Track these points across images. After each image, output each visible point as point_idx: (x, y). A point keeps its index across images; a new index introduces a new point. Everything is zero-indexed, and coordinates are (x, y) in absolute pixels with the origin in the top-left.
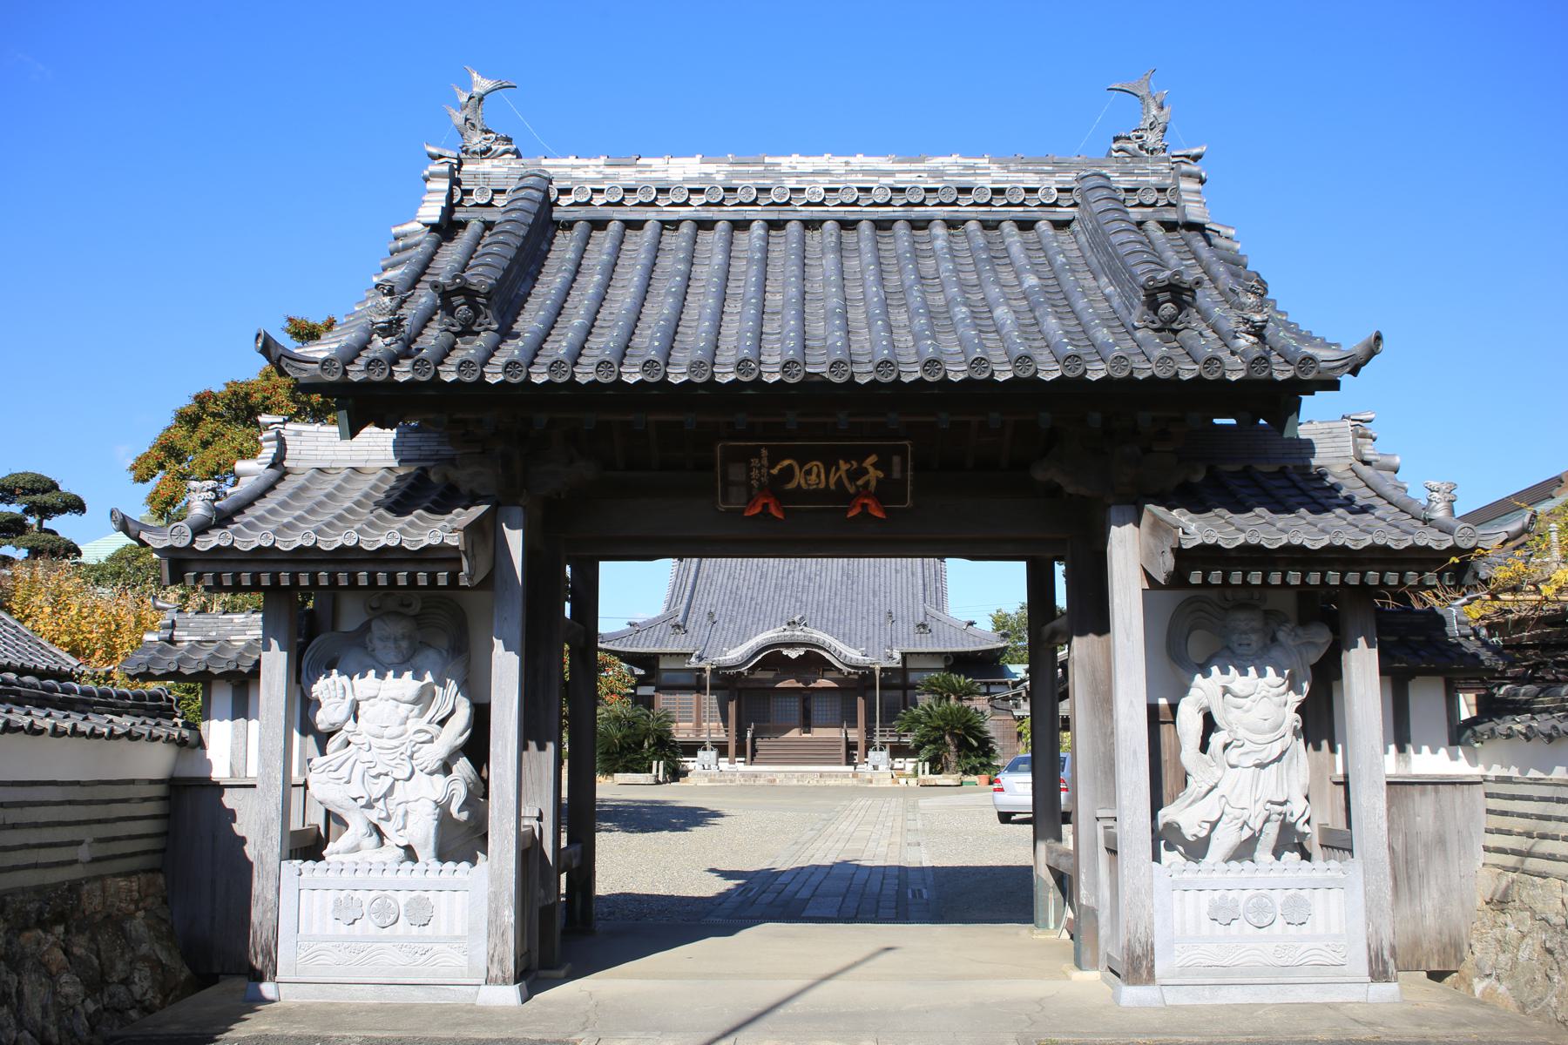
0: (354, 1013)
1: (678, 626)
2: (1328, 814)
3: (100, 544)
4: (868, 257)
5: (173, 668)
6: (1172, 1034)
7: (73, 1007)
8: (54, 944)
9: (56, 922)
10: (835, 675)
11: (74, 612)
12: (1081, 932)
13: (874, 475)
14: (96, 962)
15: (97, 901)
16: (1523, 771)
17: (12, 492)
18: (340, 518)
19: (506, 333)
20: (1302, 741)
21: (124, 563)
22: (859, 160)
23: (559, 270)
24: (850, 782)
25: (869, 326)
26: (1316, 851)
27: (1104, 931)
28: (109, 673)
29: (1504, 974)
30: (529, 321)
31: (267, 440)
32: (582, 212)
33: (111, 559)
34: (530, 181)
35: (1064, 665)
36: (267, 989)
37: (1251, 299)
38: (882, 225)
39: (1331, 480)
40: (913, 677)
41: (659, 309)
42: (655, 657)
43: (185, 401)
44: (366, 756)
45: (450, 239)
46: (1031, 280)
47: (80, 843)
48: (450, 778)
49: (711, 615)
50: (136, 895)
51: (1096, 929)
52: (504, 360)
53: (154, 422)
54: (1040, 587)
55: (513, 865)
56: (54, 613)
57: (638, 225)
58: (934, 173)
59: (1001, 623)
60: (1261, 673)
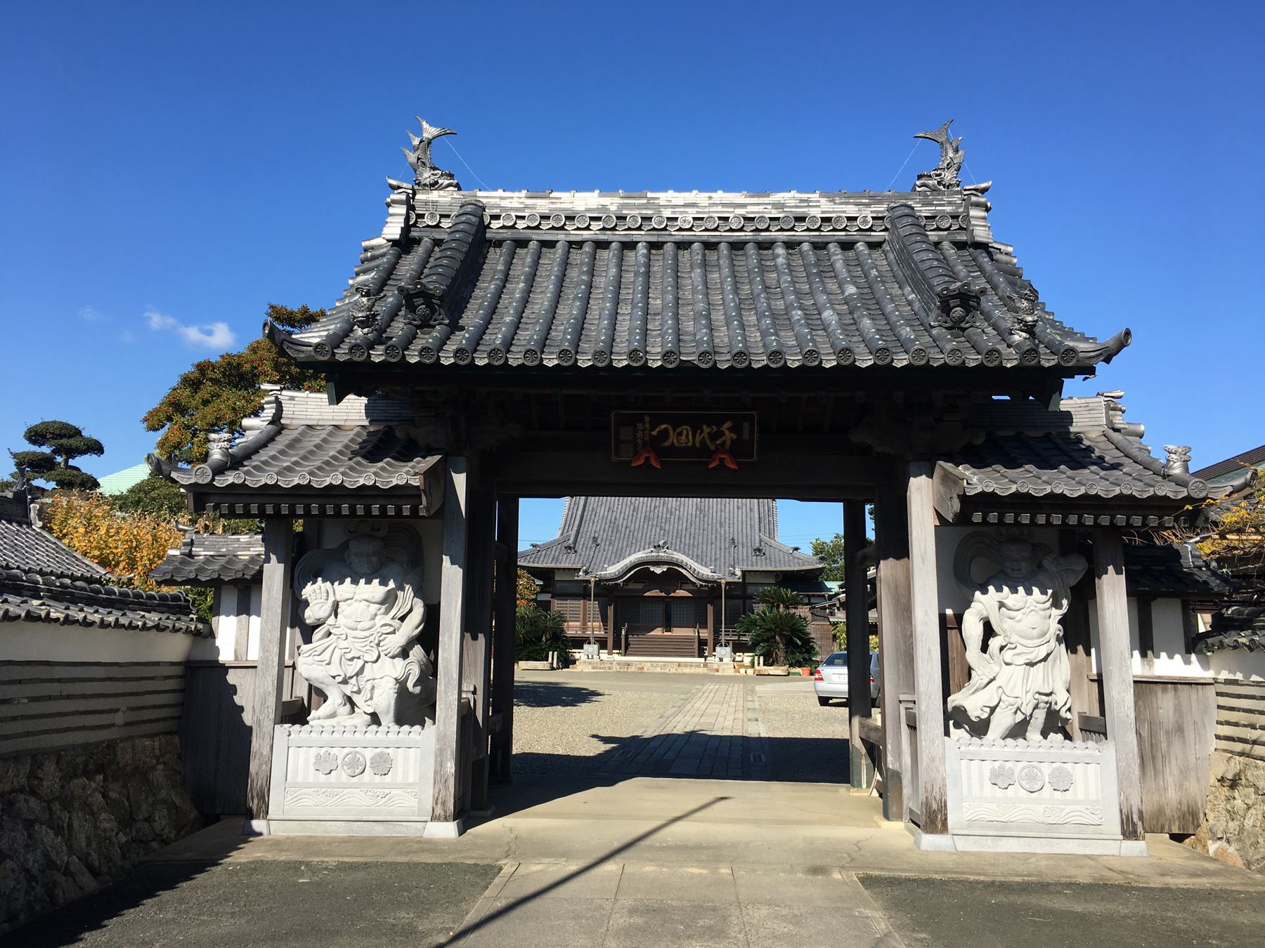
0: (329, 844)
1: (570, 548)
2: (1085, 704)
3: (120, 476)
4: (726, 271)
5: (192, 576)
6: (963, 873)
7: (109, 839)
8: (96, 789)
9: (98, 772)
10: (691, 587)
11: (103, 531)
12: (889, 790)
13: (729, 436)
14: (126, 803)
15: (128, 756)
16: (1247, 676)
17: (44, 436)
18: (327, 463)
19: (455, 327)
20: (1063, 646)
21: (142, 495)
22: (719, 196)
23: (493, 279)
24: (702, 670)
25: (728, 325)
26: (1077, 733)
27: (907, 791)
28: (130, 579)
29: (1233, 838)
30: (472, 317)
31: (268, 403)
32: (508, 234)
33: (131, 491)
34: (469, 208)
35: (873, 582)
36: (257, 825)
37: (1025, 304)
38: (737, 246)
39: (1086, 442)
40: (750, 590)
41: (569, 310)
42: (552, 570)
43: (188, 368)
44: (343, 644)
45: (408, 253)
46: (851, 290)
47: (117, 710)
48: (407, 661)
49: (595, 539)
50: (157, 752)
51: (901, 788)
52: (454, 347)
53: (159, 387)
54: (853, 523)
55: (454, 728)
56: (87, 532)
57: (551, 244)
58: (777, 206)
59: (819, 549)
60: (1029, 592)
